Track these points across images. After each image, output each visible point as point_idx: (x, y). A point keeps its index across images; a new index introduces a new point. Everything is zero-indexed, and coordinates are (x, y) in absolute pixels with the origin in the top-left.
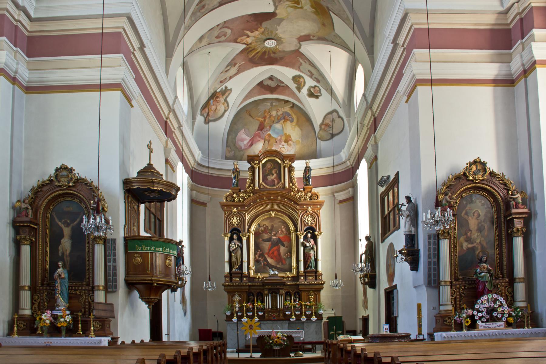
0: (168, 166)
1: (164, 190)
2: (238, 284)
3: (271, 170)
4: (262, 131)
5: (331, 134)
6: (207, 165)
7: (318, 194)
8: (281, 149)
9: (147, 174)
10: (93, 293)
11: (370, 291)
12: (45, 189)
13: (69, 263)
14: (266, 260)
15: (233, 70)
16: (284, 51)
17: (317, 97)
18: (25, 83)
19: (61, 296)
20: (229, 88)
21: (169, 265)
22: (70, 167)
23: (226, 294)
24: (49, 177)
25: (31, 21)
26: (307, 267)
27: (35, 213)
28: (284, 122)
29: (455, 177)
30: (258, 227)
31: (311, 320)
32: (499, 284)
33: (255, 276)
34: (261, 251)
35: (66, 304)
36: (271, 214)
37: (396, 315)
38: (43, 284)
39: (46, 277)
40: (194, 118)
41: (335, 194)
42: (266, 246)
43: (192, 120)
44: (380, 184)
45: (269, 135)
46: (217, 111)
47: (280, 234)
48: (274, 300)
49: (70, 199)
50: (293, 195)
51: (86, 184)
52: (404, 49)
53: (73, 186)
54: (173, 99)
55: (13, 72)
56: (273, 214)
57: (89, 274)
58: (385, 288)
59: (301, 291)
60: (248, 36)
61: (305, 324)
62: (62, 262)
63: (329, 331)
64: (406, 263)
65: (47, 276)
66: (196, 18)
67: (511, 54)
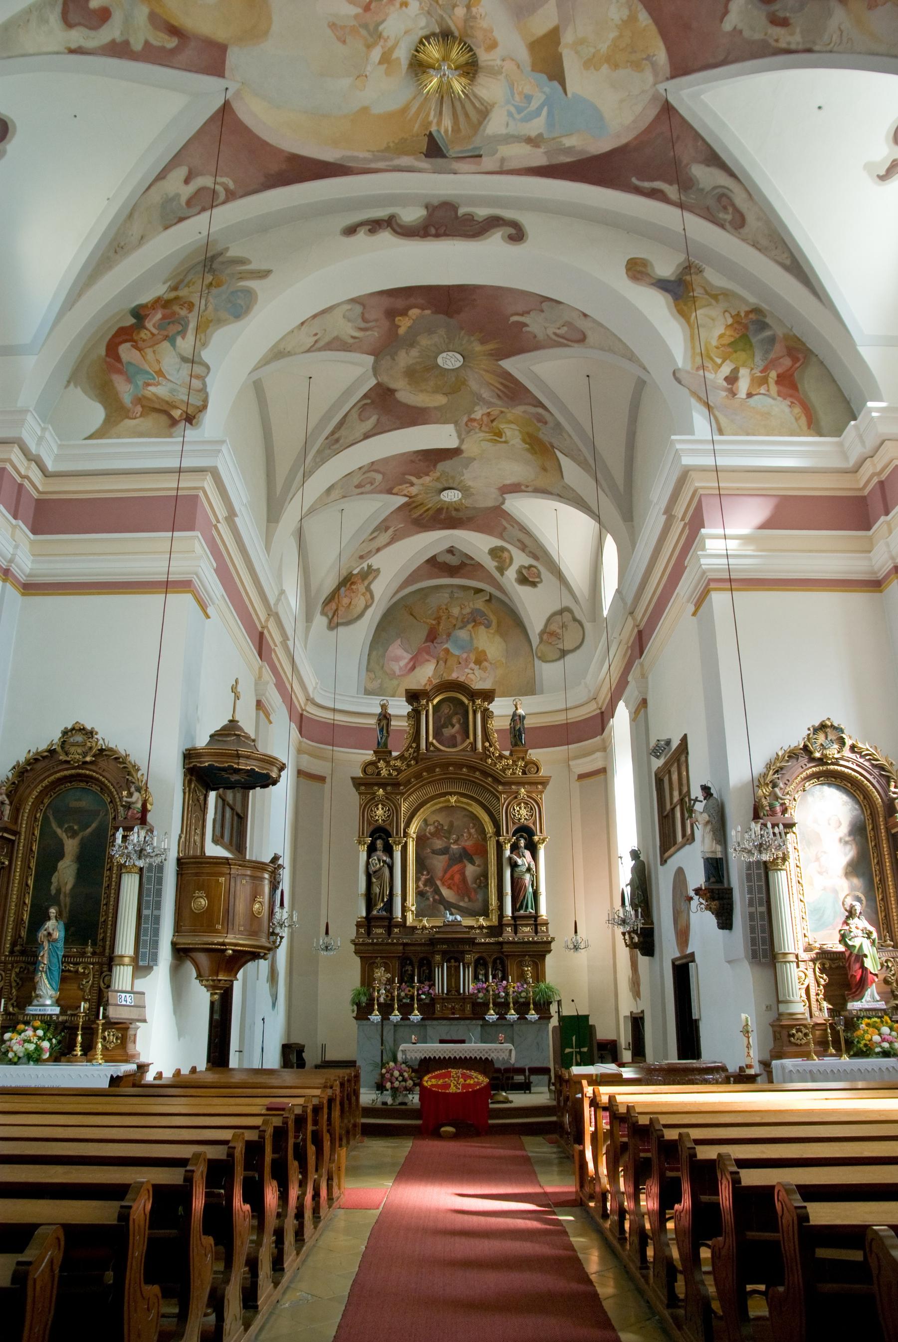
0: (261, 713)
1: (257, 770)
2: (383, 941)
3: (449, 718)
4: (433, 642)
5: (560, 649)
6: (330, 705)
7: (538, 764)
8: (469, 676)
9: (229, 739)
10: (110, 970)
11: (643, 960)
12: (39, 766)
13: (67, 910)
14: (437, 891)
15: (384, 538)
16: (475, 508)
17: (534, 584)
18: (22, 576)
19: (47, 975)
20: (375, 567)
21: (259, 913)
22: (89, 727)
23: (358, 960)
24: (48, 746)
25: (46, 476)
26: (518, 906)
27: (16, 811)
28: (473, 627)
29: (789, 752)
30: (423, 825)
31: (526, 1018)
32: (890, 961)
33: (415, 924)
34: (428, 874)
35: (54, 993)
36: (449, 801)
37: (697, 1017)
38: (12, 952)
39: (20, 937)
40: (309, 618)
41: (571, 763)
42: (439, 863)
43: (305, 624)
44: (653, 754)
45: (447, 651)
46: (351, 608)
47: (466, 841)
48: (453, 975)
49: (83, 785)
50: (491, 764)
51: (116, 758)
52: (685, 525)
53: (91, 763)
54: (277, 594)
55: (5, 560)
56: (453, 799)
57: (105, 932)
58: (673, 957)
59: (507, 956)
60: (412, 484)
61: (516, 1028)
62: (57, 908)
63: (563, 1049)
64: (709, 913)
65: (23, 934)
66: (322, 458)
67: (870, 538)
